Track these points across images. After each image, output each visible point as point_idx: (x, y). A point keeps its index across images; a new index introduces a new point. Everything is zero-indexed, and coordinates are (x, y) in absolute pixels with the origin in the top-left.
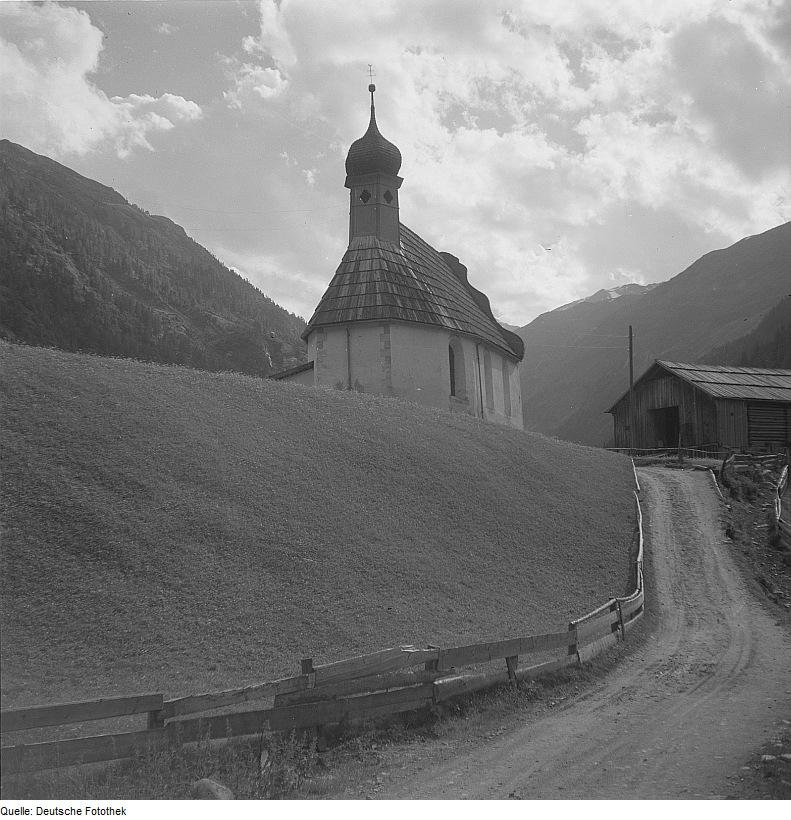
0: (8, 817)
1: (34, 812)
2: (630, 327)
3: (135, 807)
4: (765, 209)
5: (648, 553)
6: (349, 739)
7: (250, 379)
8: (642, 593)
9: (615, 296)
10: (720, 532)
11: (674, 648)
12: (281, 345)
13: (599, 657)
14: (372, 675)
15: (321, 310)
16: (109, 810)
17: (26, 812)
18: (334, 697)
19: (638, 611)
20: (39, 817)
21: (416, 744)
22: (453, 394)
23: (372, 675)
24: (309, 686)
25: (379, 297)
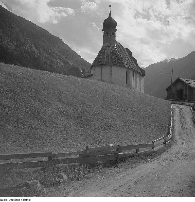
0: (2, 201)
1: (8, 200)
2: (172, 69)
3: (34, 199)
5: (173, 125)
8: (171, 135)
9: (169, 61)
13: (159, 150)
16: (27, 200)
17: (6, 200)
20: (10, 201)
22: (127, 84)
25: (109, 59)
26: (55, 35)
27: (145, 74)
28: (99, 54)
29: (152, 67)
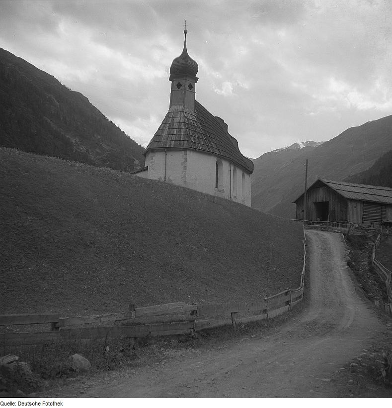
0: (4, 407)
1: (17, 404)
2: (307, 160)
3: (67, 402)
4: (370, 103)
5: (308, 271)
6: (150, 345)
7: (115, 171)
8: (303, 289)
9: (302, 146)
10: (344, 263)
11: (317, 316)
12: (134, 160)
13: (278, 317)
14: (163, 315)
15: (153, 141)
16: (54, 403)
17: (13, 404)
18: (144, 324)
19: (300, 297)
20: (19, 407)
21: (184, 350)
22: (216, 187)
23: (163, 315)
24: (132, 317)
25: (182, 136)
26: (74, 88)
27: (253, 169)
28: (162, 126)
29: (267, 157)
